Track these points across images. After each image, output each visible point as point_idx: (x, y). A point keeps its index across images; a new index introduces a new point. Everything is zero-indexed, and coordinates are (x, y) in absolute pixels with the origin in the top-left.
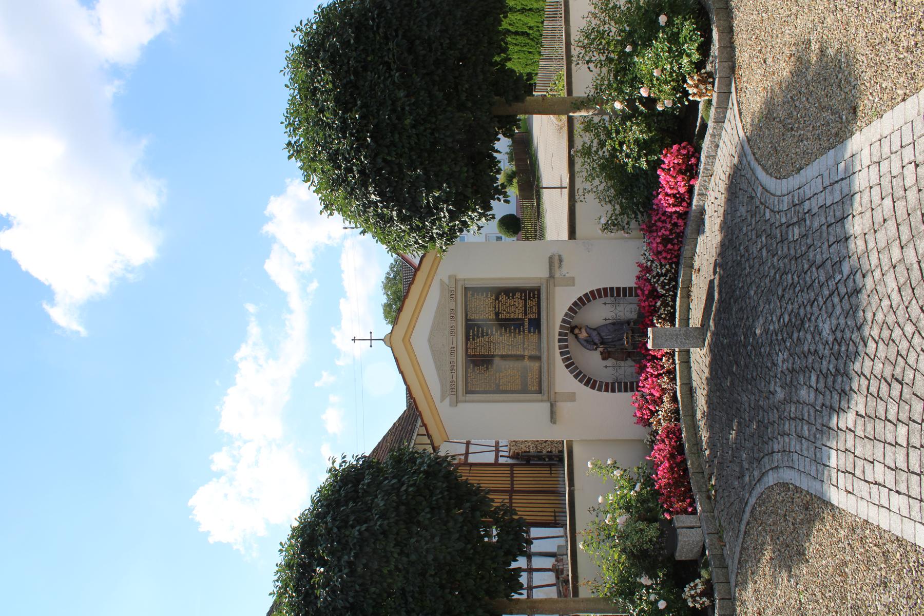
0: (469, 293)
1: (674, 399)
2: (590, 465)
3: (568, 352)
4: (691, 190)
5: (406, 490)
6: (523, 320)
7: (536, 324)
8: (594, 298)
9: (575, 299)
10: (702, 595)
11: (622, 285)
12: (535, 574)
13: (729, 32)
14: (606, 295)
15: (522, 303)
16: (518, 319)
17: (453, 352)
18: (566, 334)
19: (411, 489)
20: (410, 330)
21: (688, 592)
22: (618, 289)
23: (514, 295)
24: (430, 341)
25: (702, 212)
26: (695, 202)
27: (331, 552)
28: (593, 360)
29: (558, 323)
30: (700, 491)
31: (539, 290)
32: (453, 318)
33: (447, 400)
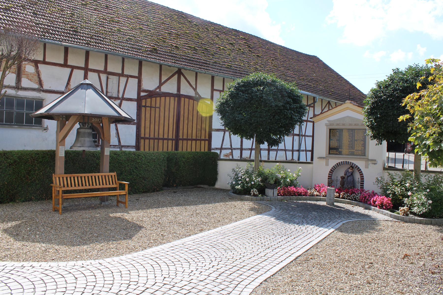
0: (364, 131)
1: (317, 196)
2: (300, 168)
3: (346, 164)
4: (376, 206)
5: (285, 112)
6: (354, 149)
7: (352, 154)
8: (360, 175)
9: (360, 168)
10: (254, 193)
11: (364, 185)
12: (291, 152)
13: (420, 222)
14: (361, 179)
15: (360, 149)
16: (354, 147)
17: (344, 125)
18: (350, 165)
19: (285, 113)
20: (343, 110)
21: (255, 190)
22: (363, 183)
23: (363, 147)
24: (348, 117)
25: (370, 209)
26: (373, 207)
27: (267, 91)
28: (341, 173)
29: (352, 162)
30: (284, 198)
31: (365, 155)
32: (355, 125)
33: (327, 122)
